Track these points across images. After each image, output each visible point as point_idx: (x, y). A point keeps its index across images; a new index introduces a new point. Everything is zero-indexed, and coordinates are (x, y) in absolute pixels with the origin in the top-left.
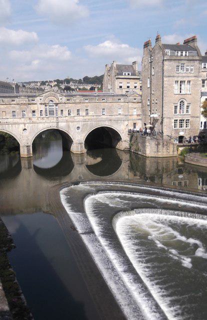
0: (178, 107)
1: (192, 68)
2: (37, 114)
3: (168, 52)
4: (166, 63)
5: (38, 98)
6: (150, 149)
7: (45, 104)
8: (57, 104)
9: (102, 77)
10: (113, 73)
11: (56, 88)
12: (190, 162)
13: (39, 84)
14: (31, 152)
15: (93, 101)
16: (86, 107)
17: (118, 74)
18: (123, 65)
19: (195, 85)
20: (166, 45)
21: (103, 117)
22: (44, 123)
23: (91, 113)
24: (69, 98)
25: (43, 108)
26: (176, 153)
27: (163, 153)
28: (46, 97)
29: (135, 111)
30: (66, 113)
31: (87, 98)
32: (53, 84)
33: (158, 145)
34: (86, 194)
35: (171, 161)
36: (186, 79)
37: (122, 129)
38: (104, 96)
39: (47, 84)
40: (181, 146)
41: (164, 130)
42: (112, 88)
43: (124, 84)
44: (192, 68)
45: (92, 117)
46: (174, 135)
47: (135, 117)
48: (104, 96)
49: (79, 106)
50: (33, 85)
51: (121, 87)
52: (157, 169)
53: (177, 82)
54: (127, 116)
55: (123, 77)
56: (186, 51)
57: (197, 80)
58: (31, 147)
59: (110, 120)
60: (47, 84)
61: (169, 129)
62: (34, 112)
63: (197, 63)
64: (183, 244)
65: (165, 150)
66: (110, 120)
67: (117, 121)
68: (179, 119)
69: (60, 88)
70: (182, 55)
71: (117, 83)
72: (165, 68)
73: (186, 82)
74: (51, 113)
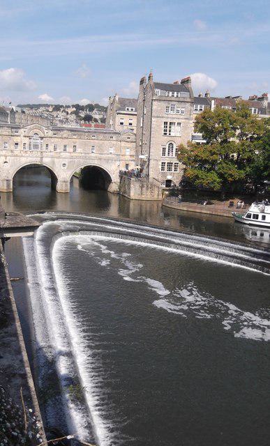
0: (167, 150)
1: (184, 109)
2: (20, 147)
3: (158, 92)
4: (154, 103)
5: (22, 130)
6: (134, 192)
7: (30, 138)
8: (42, 138)
9: (107, 108)
10: (117, 105)
11: (73, 117)
12: (222, 214)
13: (51, 109)
14: (12, 187)
15: (82, 137)
16: (75, 143)
17: (120, 109)
18: (128, 99)
19: (186, 128)
20: (169, 85)
21: (92, 155)
22: (27, 157)
23: (79, 150)
24: (55, 132)
25: (26, 140)
26: (161, 197)
27: (147, 195)
28: (31, 129)
29: (128, 152)
30: (51, 148)
31: (76, 133)
32: (70, 110)
33: (142, 187)
34: (45, 220)
35: (155, 205)
36: (176, 121)
37: (113, 170)
38: (95, 132)
39: (62, 109)
40: (167, 190)
41: (151, 173)
42: (114, 124)
43: (126, 120)
44: (184, 109)
45: (80, 155)
46: (160, 178)
47: (128, 158)
48: (95, 132)
49: (66, 142)
50: (42, 109)
51: (122, 124)
52: (141, 214)
53: (166, 123)
54: (119, 156)
55: (125, 112)
56: (178, 92)
57: (189, 123)
58: (12, 182)
59: (100, 159)
60: (62, 109)
61: (155, 172)
62: (17, 144)
63: (188, 105)
64: (104, 263)
65: (149, 193)
66: (100, 159)
67: (107, 160)
68: (166, 162)
69: (78, 116)
70: (173, 96)
71: (118, 119)
72: (154, 107)
73: (176, 124)
74: (36, 146)
